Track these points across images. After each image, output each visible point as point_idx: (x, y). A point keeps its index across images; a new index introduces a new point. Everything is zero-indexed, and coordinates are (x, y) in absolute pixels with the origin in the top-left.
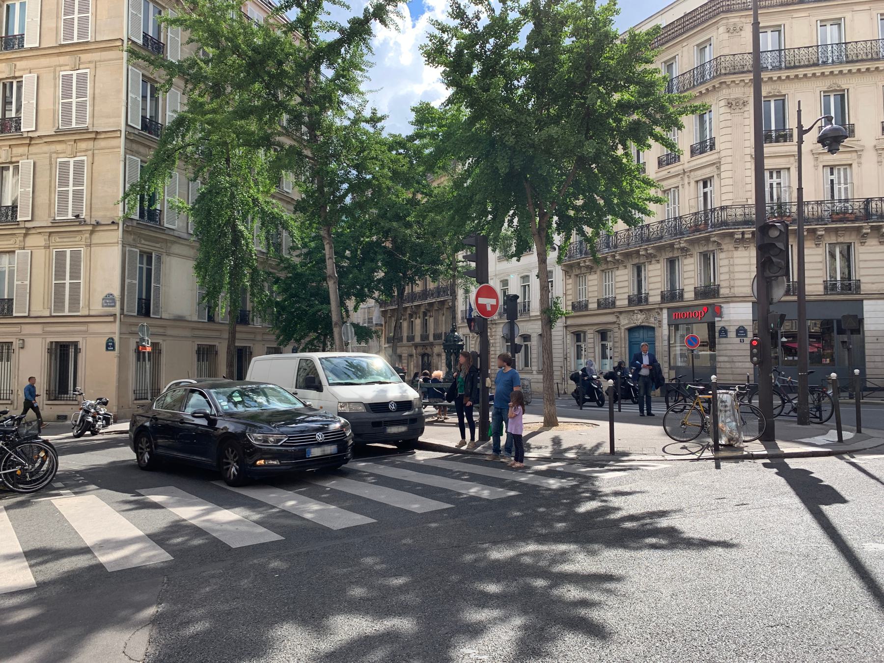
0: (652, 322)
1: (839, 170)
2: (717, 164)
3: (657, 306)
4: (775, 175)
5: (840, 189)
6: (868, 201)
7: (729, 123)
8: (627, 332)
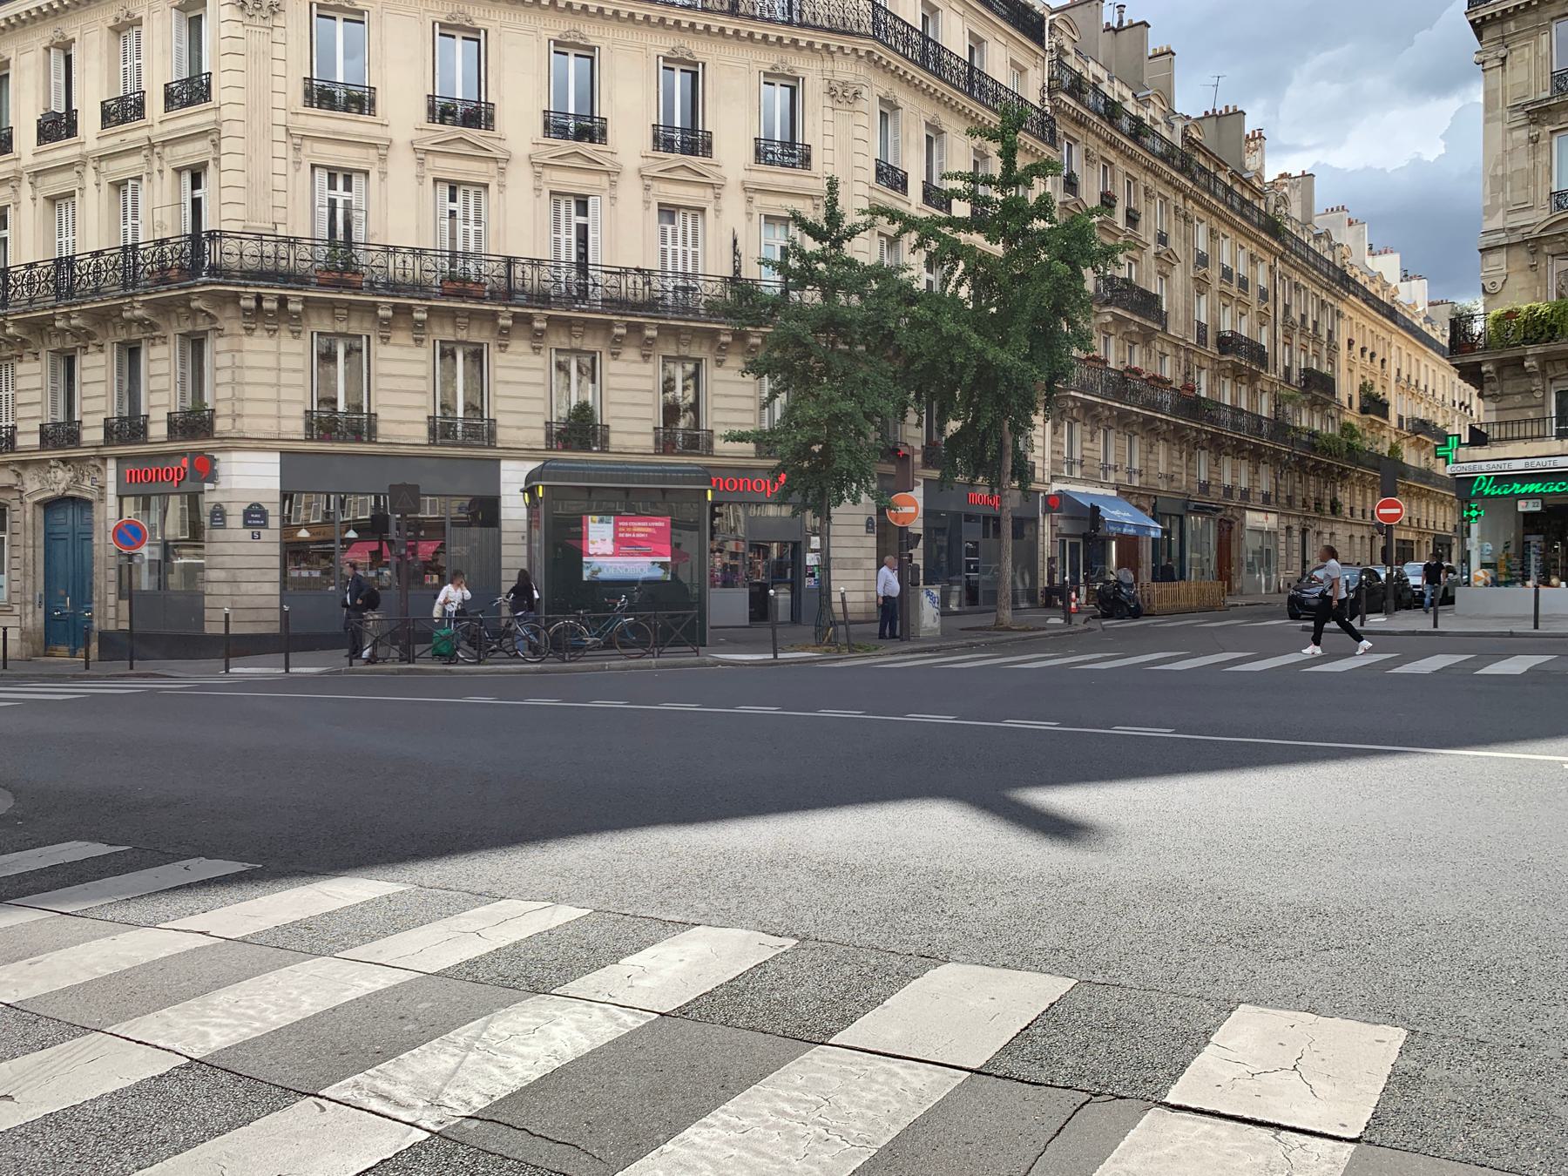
0: (87, 489)
1: (466, 192)
2: (211, 135)
3: (92, 452)
4: (340, 183)
5: (466, 232)
6: (510, 262)
7: (239, 46)
8: (40, 512)
